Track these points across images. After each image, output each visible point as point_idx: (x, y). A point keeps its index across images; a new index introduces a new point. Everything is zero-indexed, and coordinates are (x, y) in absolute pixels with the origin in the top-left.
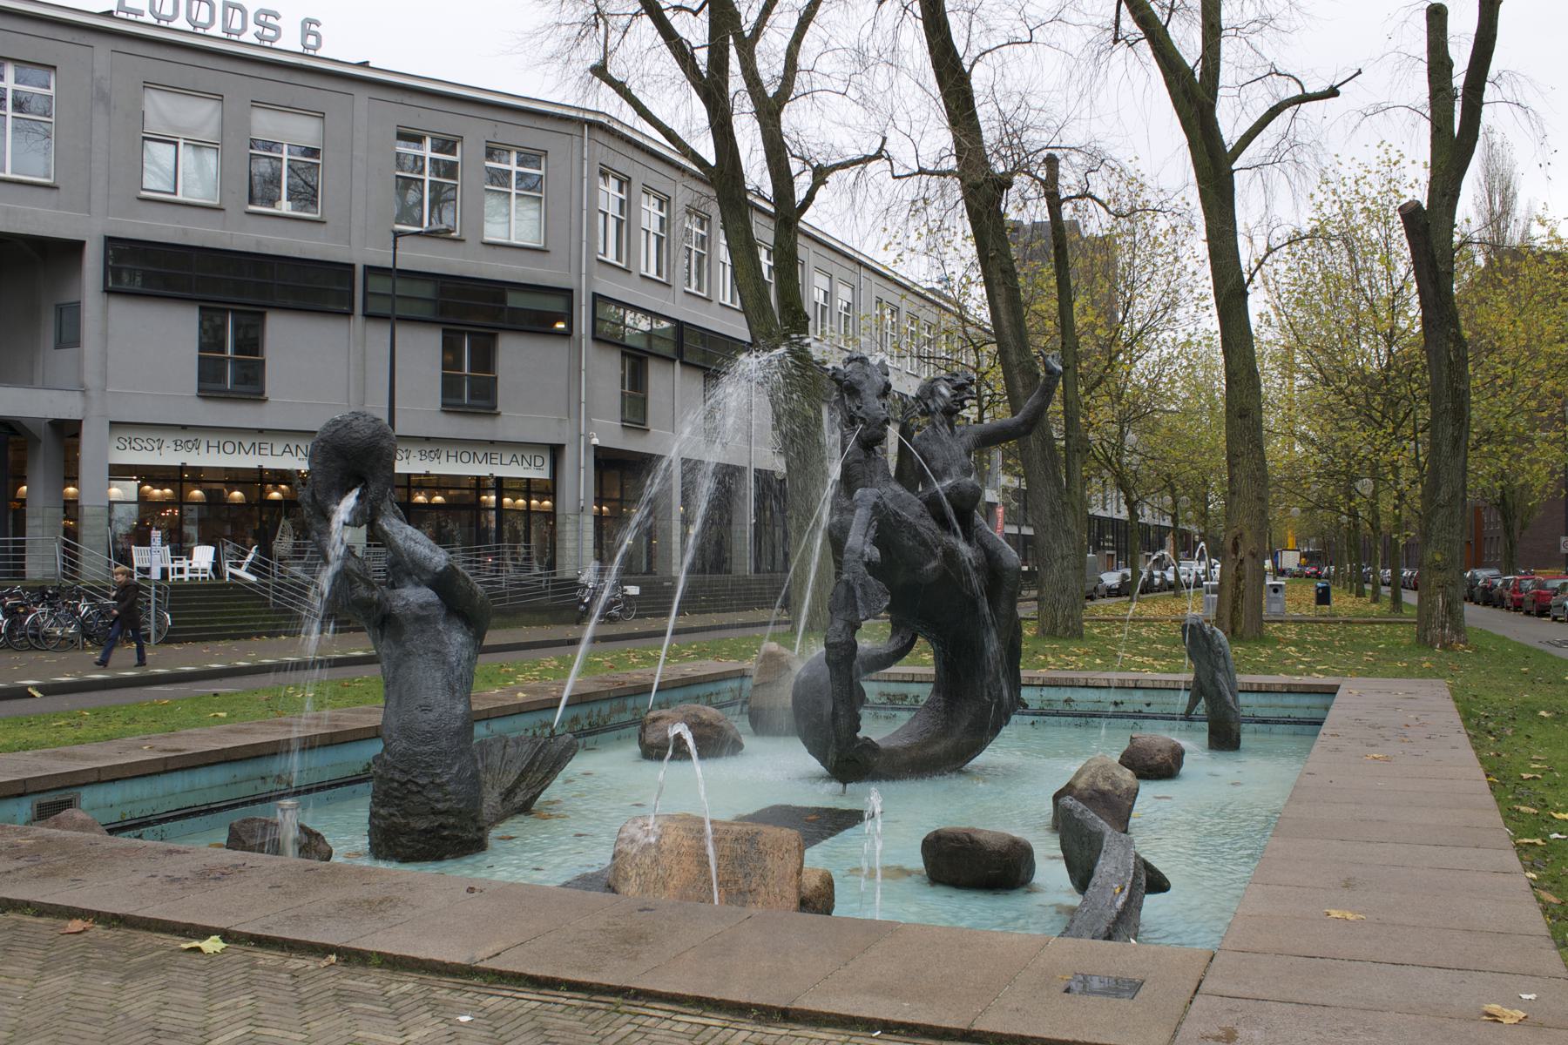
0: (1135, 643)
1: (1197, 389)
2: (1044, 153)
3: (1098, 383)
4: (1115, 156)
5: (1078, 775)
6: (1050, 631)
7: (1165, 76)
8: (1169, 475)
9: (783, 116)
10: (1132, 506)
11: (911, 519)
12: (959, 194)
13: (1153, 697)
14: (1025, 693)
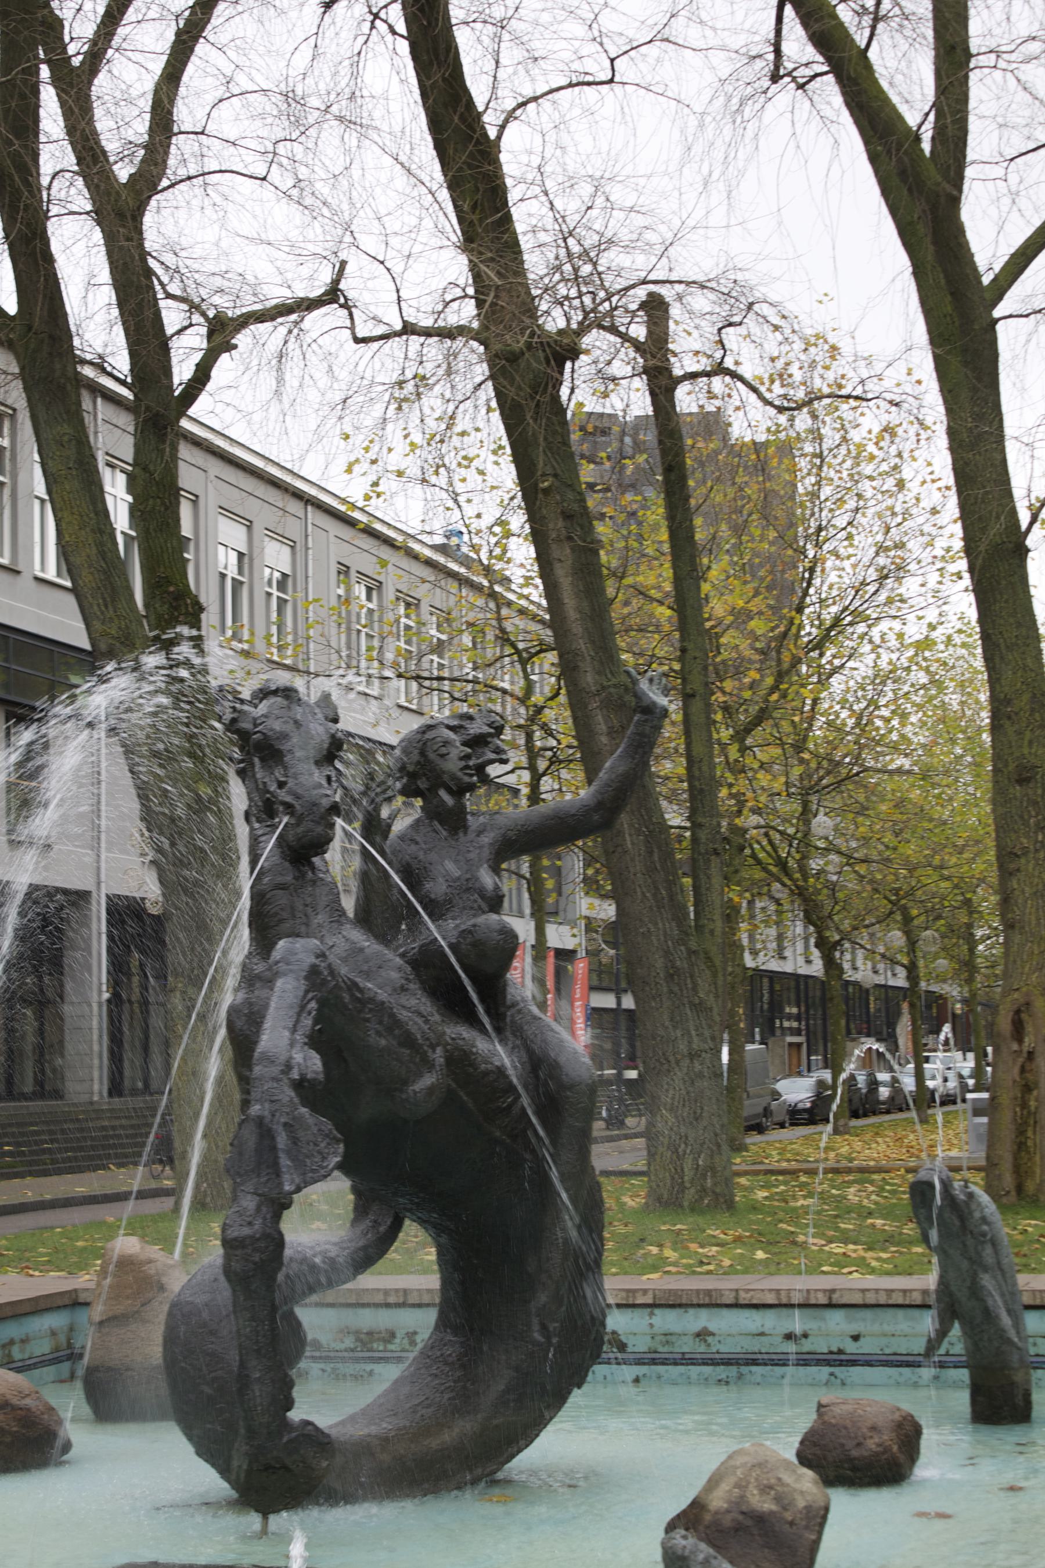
0: (835, 1216)
1: (946, 724)
2: (641, 293)
3: (758, 720)
4: (773, 297)
5: (713, 1482)
6: (667, 1200)
7: (867, 143)
8: (896, 891)
9: (149, 219)
10: (827, 949)
11: (382, 995)
12: (482, 370)
13: (864, 1322)
14: (616, 1322)
